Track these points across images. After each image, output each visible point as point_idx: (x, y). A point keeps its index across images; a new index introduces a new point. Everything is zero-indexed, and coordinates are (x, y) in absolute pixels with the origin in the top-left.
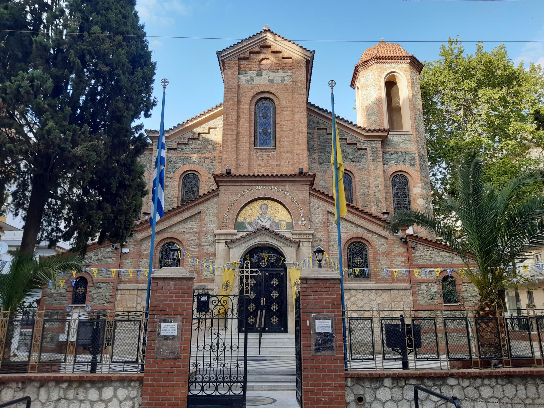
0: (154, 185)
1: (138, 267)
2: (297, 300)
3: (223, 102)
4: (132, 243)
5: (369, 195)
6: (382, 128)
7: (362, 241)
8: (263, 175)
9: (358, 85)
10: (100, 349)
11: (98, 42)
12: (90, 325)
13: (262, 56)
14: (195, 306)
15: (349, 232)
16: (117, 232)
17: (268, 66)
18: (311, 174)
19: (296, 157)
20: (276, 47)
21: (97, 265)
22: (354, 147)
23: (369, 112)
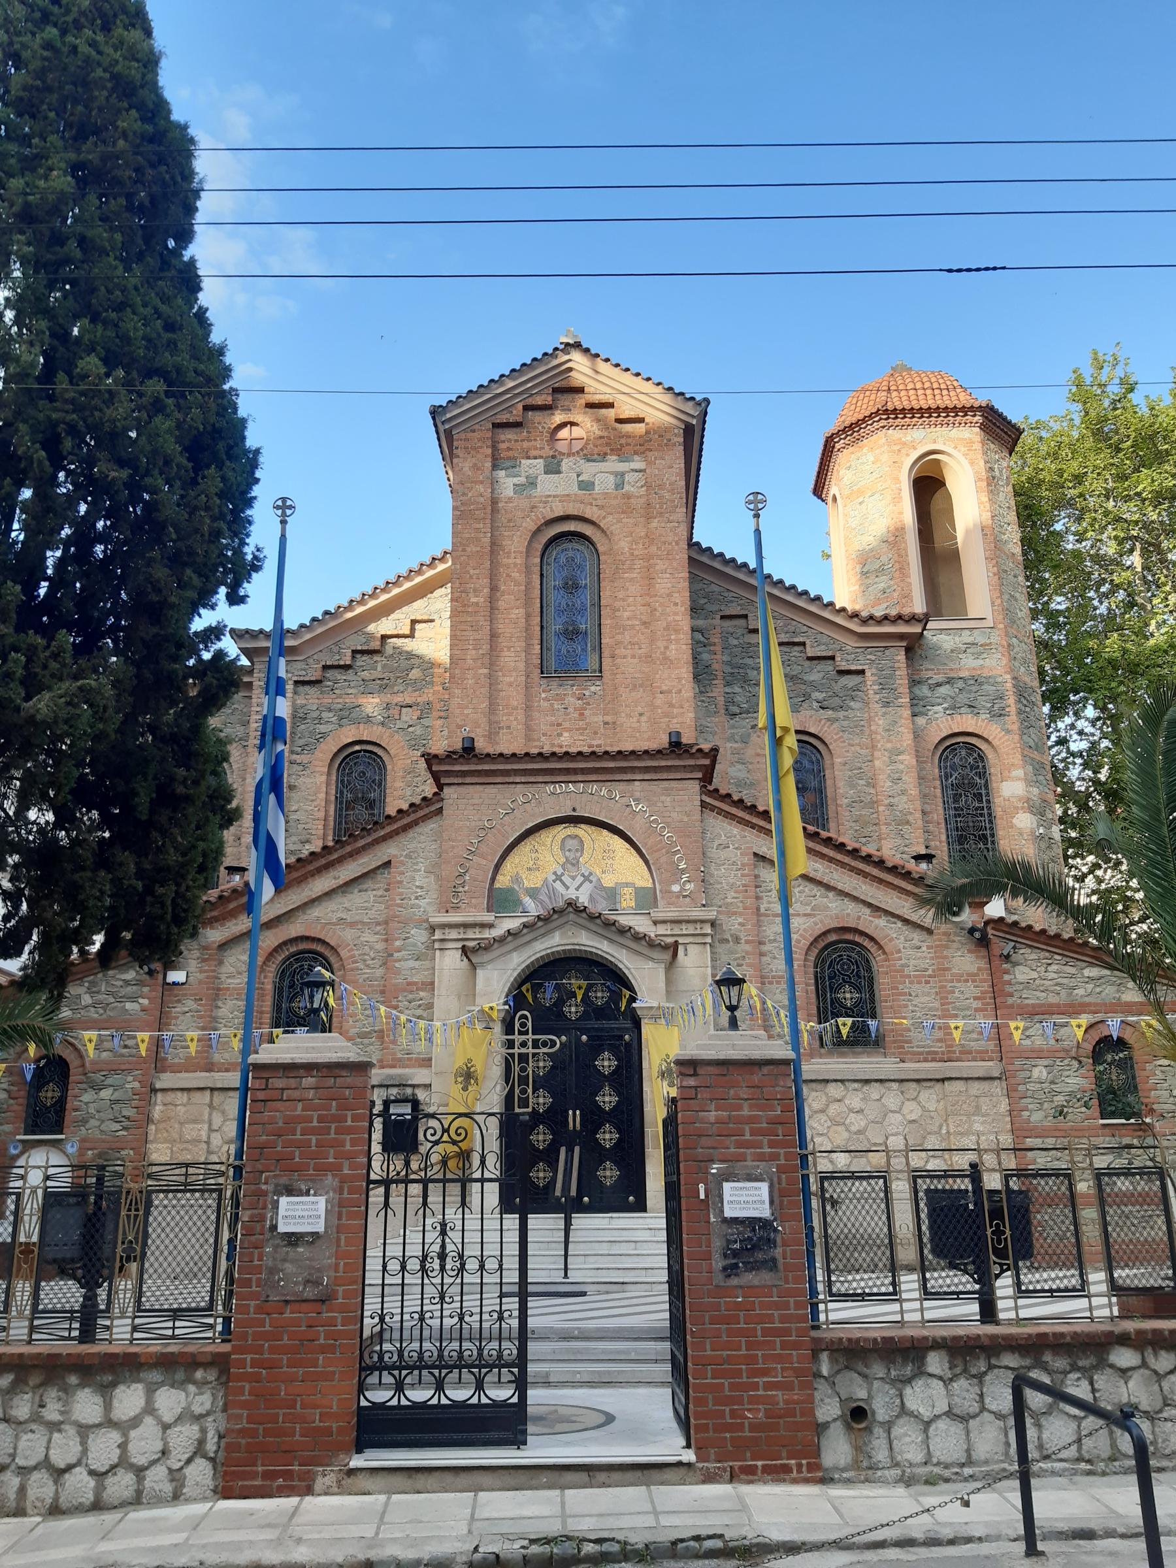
0: (258, 801)
1: (211, 1023)
2: (670, 1123)
3: (449, 548)
4: (196, 954)
5: (874, 803)
6: (906, 611)
7: (857, 939)
8: (567, 753)
9: (833, 489)
10: (105, 1272)
11: (96, 401)
12: (78, 1204)
13: (558, 418)
14: (377, 1136)
15: (815, 914)
16: (153, 931)
17: (577, 446)
18: (706, 747)
19: (660, 700)
20: (597, 390)
21: (95, 1021)
22: (828, 666)
23: (868, 566)
